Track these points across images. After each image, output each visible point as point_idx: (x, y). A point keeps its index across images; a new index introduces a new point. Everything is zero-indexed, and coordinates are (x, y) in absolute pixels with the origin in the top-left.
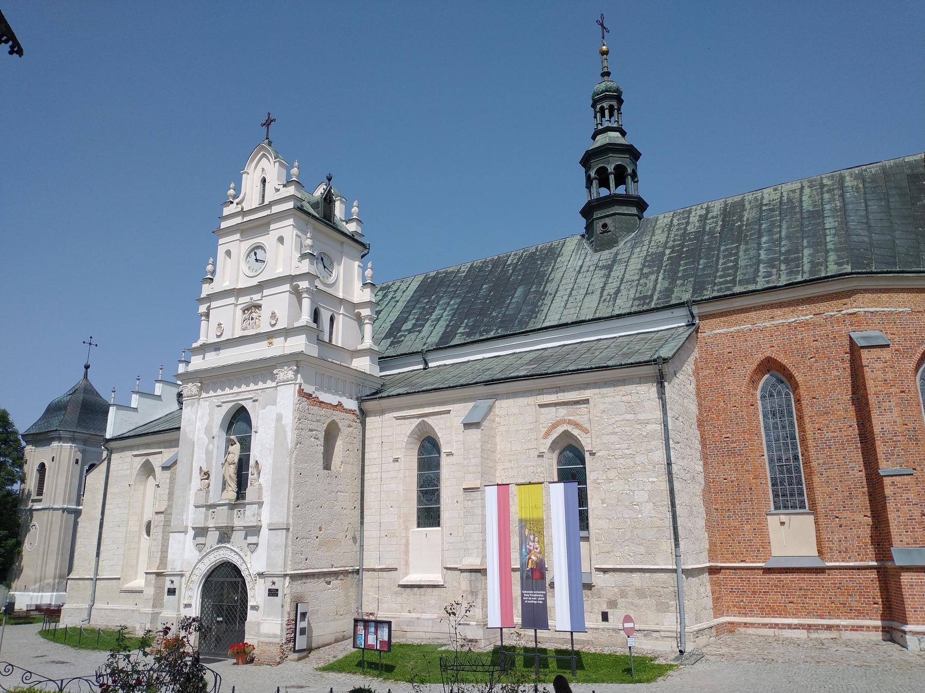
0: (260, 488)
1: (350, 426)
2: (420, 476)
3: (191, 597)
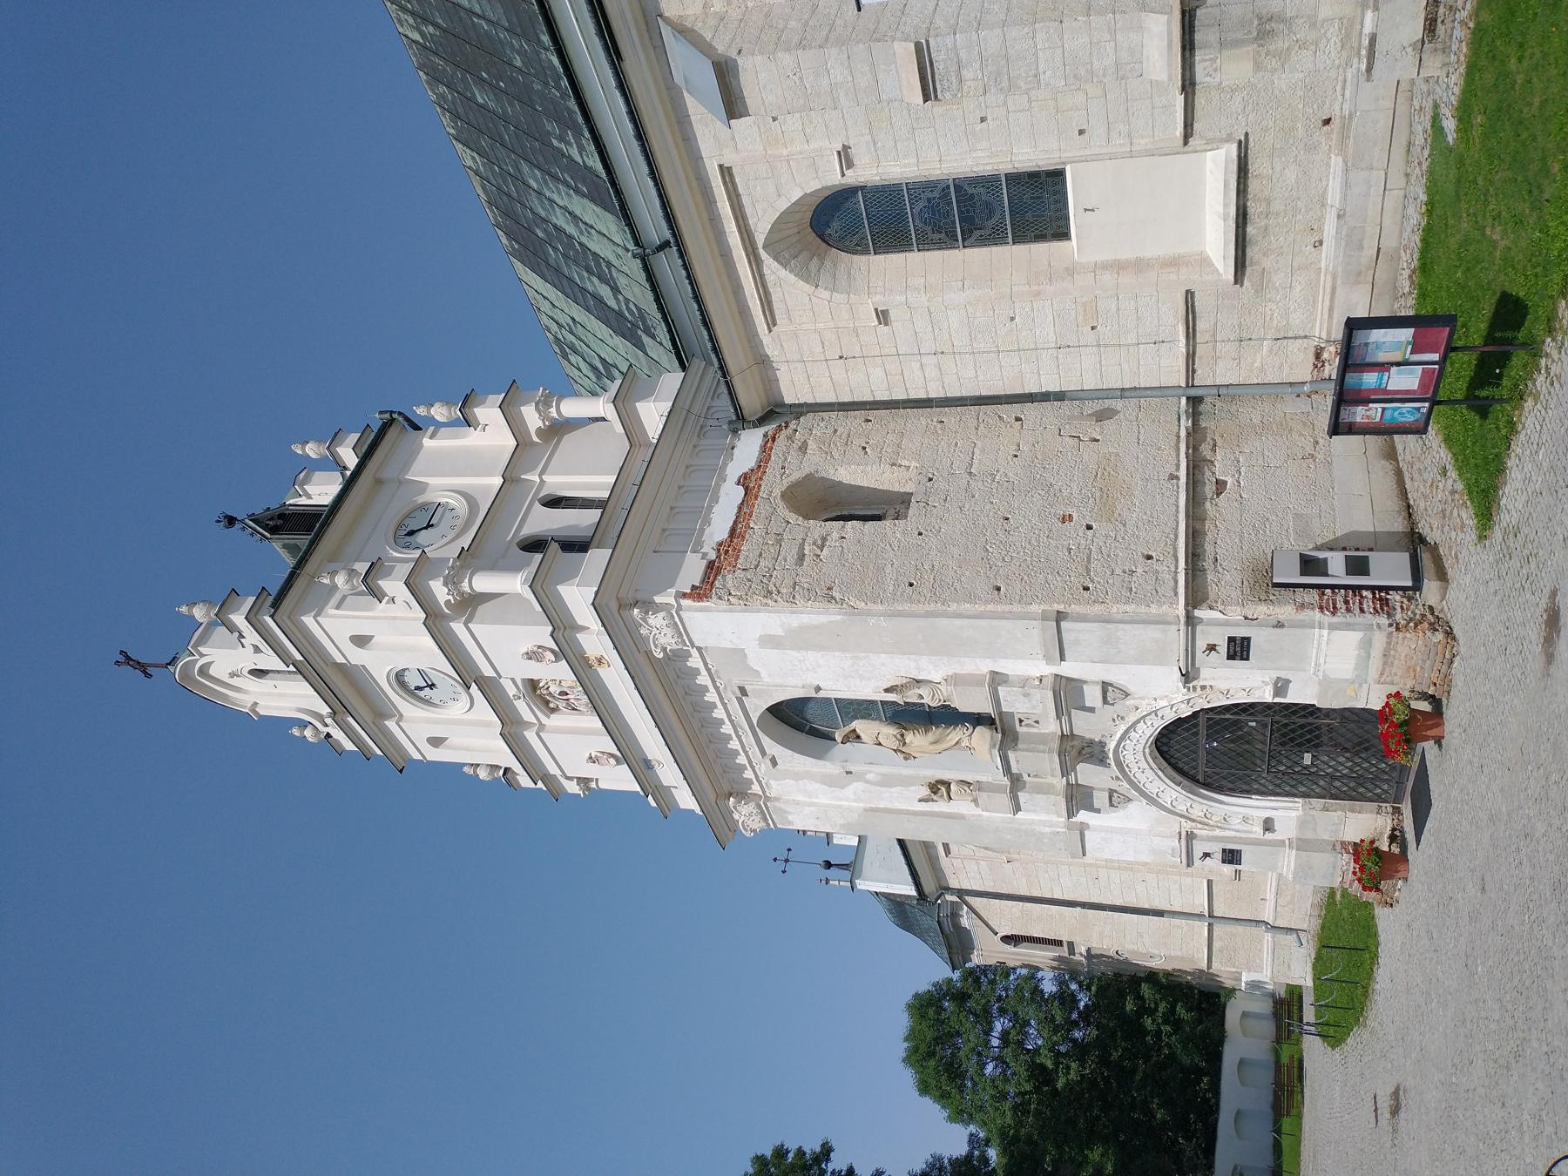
0: (955, 680)
1: (803, 448)
2: (925, 244)
3: (1245, 820)
